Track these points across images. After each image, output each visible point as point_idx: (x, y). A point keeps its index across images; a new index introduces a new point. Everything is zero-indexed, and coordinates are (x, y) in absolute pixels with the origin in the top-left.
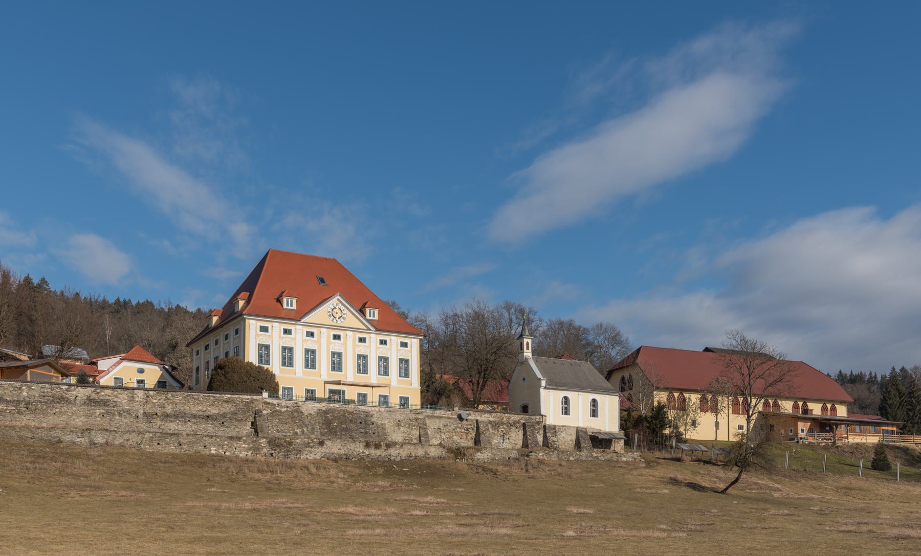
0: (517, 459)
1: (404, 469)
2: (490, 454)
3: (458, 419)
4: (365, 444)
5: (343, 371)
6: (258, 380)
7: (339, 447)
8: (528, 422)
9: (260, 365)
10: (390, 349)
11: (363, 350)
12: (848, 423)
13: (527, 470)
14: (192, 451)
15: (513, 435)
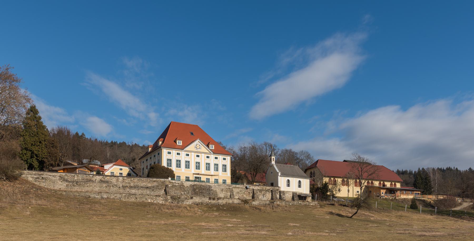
0: (269, 204)
2: (258, 202)
4: (209, 198)
10: (219, 161)
11: (208, 161)
12: (401, 190)
13: (273, 209)
14: (141, 201)
15: (267, 195)
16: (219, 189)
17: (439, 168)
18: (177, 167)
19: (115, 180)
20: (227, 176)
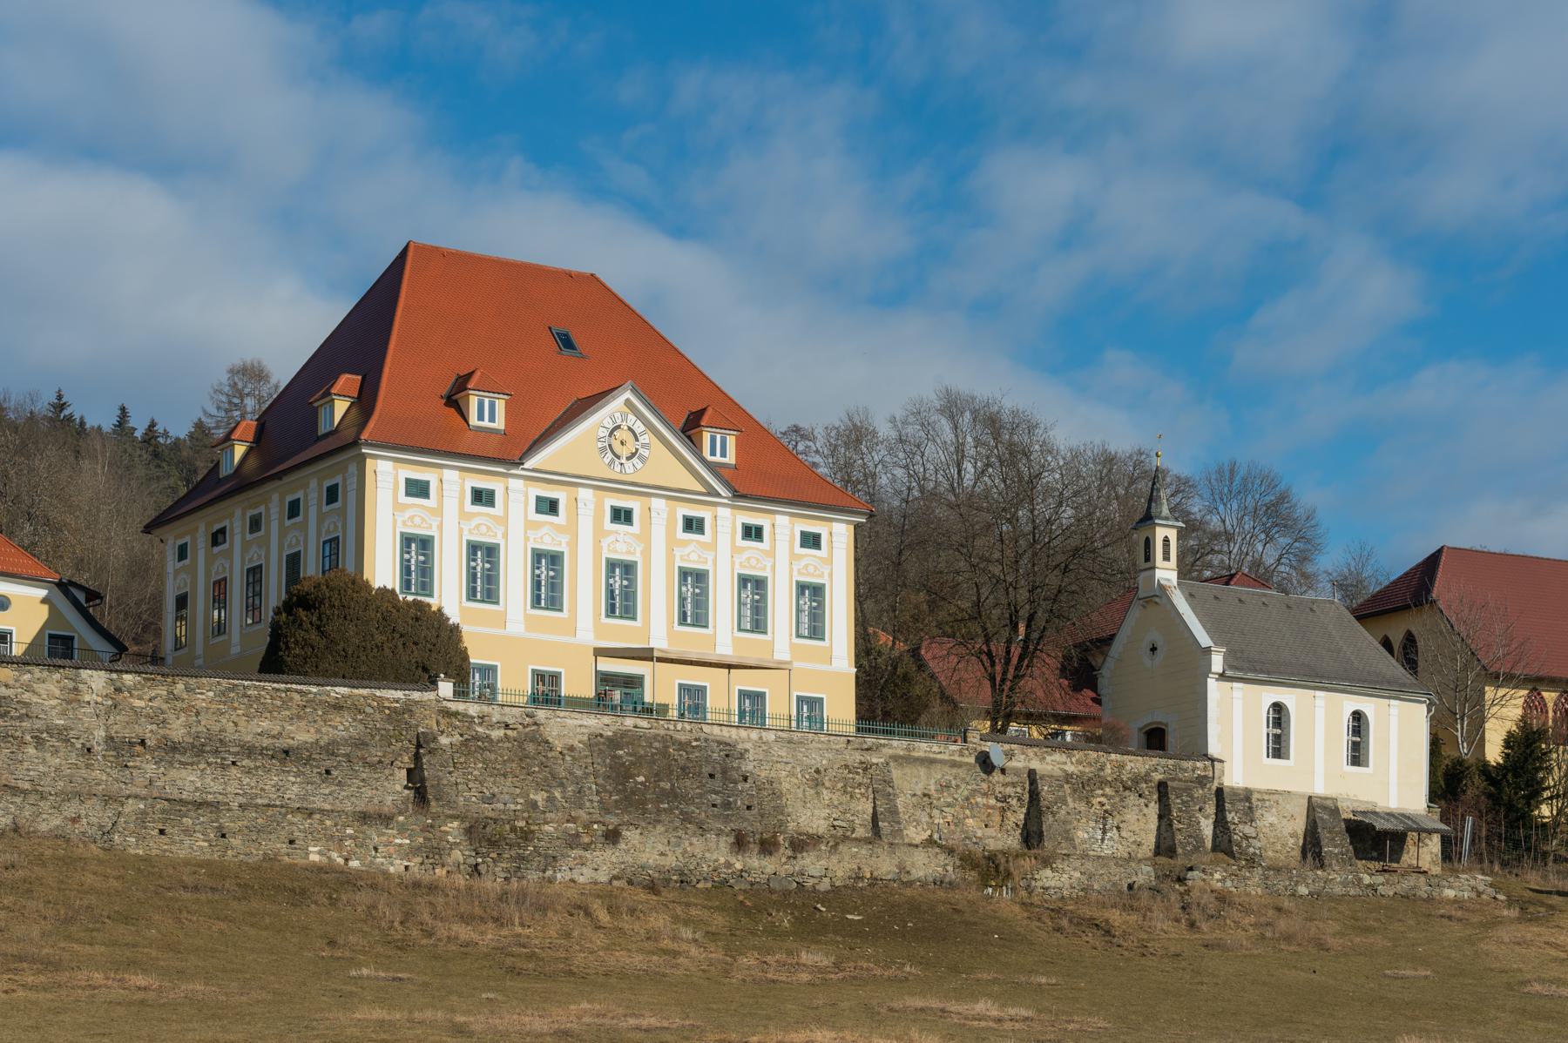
0: (1155, 890)
1: (849, 917)
2: (1077, 875)
3: (978, 769)
4: (731, 839)
5: (638, 618)
6: (416, 644)
7: (661, 847)
8: (1173, 780)
9: (419, 598)
11: (694, 557)
13: (1192, 925)
14: (257, 854)
15: (1131, 816)
16: (792, 774)
18: (472, 595)
19: (51, 696)
20: (825, 667)
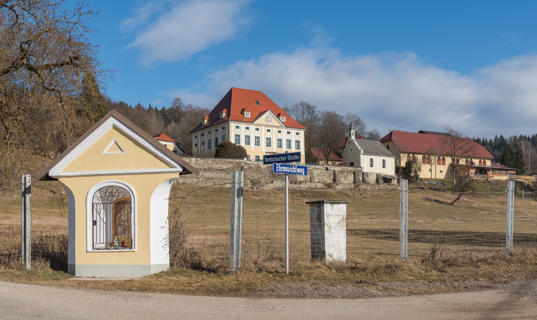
10: (292, 136)
12: (494, 169)
15: (349, 177)
17: (523, 135)
18: (246, 144)
